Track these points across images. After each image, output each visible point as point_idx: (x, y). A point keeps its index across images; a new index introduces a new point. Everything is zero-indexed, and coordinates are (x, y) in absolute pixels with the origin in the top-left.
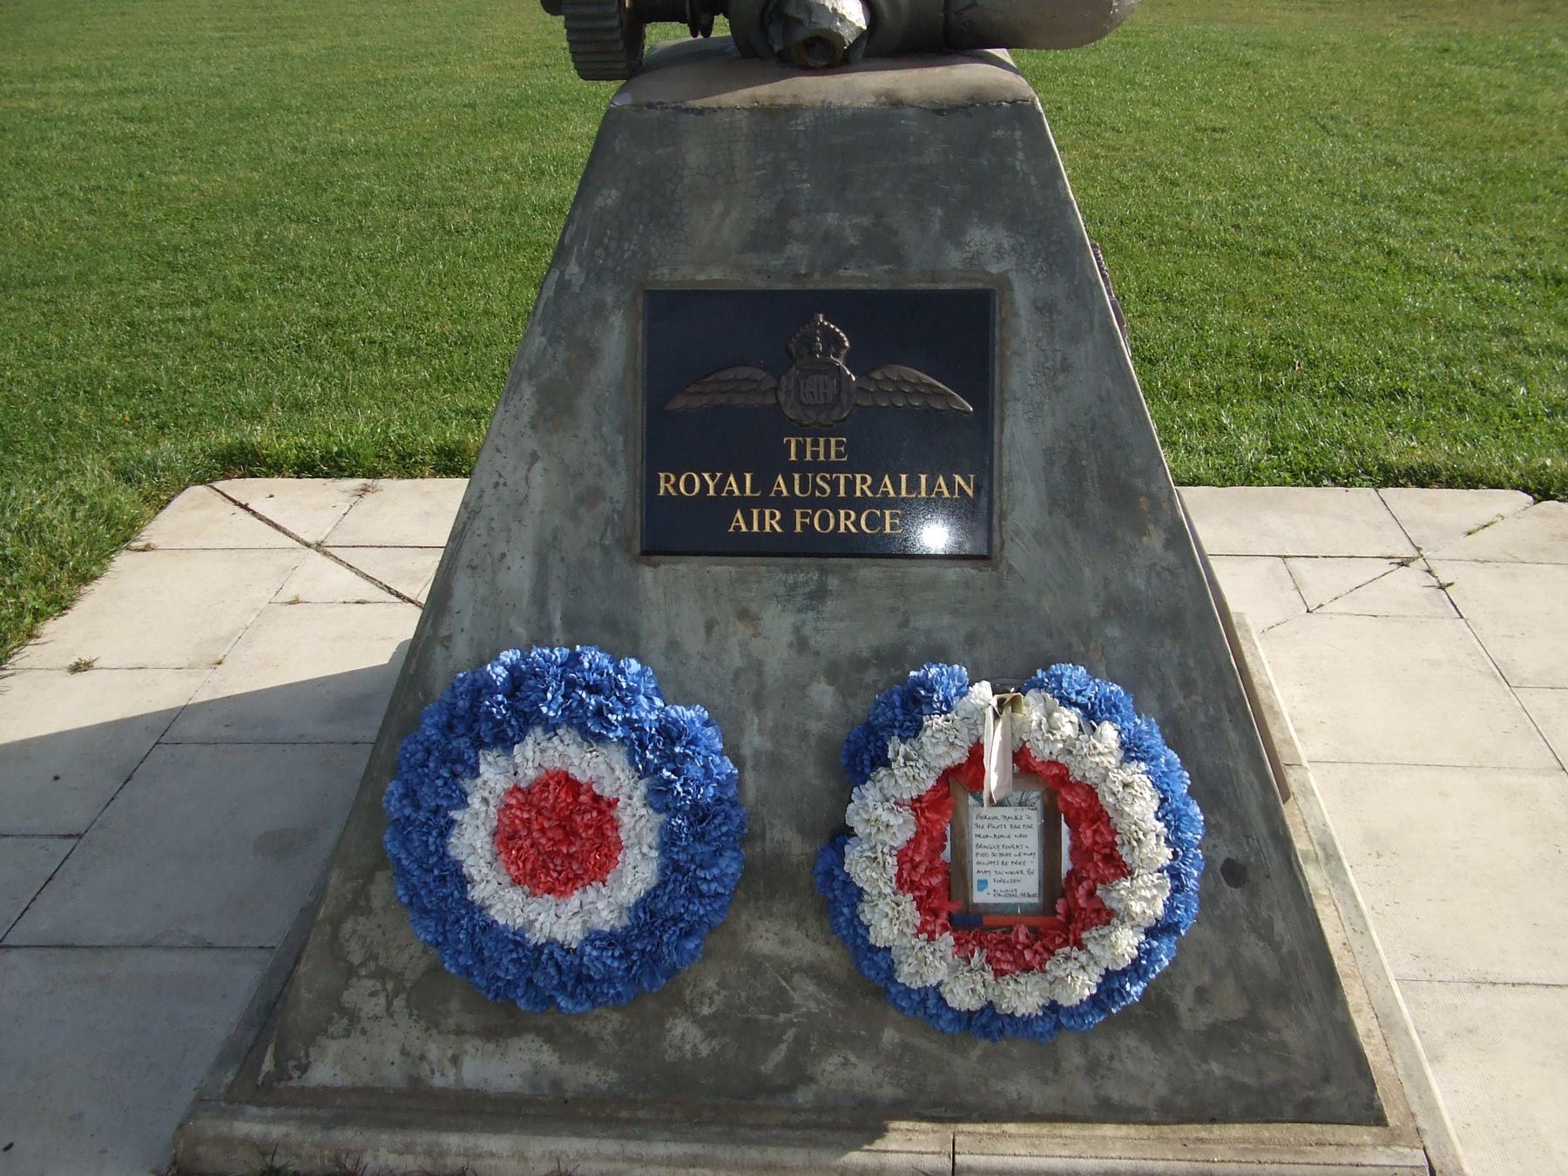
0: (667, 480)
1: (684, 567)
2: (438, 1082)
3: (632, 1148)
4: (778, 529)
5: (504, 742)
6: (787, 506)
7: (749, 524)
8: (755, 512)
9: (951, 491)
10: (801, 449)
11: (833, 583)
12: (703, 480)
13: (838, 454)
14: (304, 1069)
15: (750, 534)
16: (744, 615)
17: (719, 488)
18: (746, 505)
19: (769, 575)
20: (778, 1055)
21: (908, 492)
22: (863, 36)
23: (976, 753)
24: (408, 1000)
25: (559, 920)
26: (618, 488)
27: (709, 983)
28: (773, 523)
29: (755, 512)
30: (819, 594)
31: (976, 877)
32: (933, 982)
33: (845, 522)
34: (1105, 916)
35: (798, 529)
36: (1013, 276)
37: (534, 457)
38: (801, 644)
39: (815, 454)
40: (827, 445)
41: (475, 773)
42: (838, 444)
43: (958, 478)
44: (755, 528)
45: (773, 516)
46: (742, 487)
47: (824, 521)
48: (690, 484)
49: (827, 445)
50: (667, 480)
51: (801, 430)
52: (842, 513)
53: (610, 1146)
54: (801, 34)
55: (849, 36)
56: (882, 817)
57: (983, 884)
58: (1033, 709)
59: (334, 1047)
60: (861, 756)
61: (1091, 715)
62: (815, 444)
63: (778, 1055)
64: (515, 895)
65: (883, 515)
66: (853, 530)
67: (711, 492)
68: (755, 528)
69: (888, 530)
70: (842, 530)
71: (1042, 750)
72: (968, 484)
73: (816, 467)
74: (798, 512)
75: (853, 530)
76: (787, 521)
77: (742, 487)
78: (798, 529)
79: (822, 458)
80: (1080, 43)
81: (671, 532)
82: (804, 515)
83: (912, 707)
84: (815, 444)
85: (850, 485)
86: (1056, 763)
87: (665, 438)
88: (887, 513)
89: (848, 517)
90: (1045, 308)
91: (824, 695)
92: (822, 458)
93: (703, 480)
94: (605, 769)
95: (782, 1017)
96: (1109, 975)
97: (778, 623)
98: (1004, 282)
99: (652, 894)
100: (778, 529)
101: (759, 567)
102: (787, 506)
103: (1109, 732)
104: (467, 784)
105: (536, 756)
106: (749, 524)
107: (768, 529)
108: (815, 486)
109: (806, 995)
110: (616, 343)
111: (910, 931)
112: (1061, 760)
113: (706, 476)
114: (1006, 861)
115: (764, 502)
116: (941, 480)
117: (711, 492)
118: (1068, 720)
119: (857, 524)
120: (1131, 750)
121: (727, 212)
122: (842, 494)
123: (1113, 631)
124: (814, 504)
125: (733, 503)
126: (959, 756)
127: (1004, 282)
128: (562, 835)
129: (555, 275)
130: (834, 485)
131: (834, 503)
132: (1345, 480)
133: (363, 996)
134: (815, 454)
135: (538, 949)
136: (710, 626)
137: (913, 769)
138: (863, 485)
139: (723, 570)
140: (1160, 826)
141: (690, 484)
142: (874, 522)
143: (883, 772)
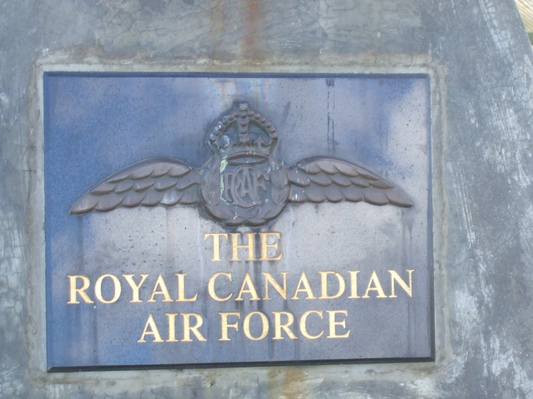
0: (80, 284)
7: (164, 334)
8: (172, 318)
9: (387, 291)
12: (123, 282)
15: (166, 345)
24: (270, 373)
28: (193, 330)
35: (225, 337)
44: (172, 338)
45: (193, 322)
47: (256, 329)
65: (326, 316)
67: (136, 298)
68: (172, 338)
69: (332, 334)
75: (87, 300)
78: (225, 337)
80: (307, 318)
82: (231, 321)
88: (332, 314)
93: (123, 282)
106: (164, 334)
107: (187, 338)
113: (129, 278)
117: (136, 298)
132: (57, 368)
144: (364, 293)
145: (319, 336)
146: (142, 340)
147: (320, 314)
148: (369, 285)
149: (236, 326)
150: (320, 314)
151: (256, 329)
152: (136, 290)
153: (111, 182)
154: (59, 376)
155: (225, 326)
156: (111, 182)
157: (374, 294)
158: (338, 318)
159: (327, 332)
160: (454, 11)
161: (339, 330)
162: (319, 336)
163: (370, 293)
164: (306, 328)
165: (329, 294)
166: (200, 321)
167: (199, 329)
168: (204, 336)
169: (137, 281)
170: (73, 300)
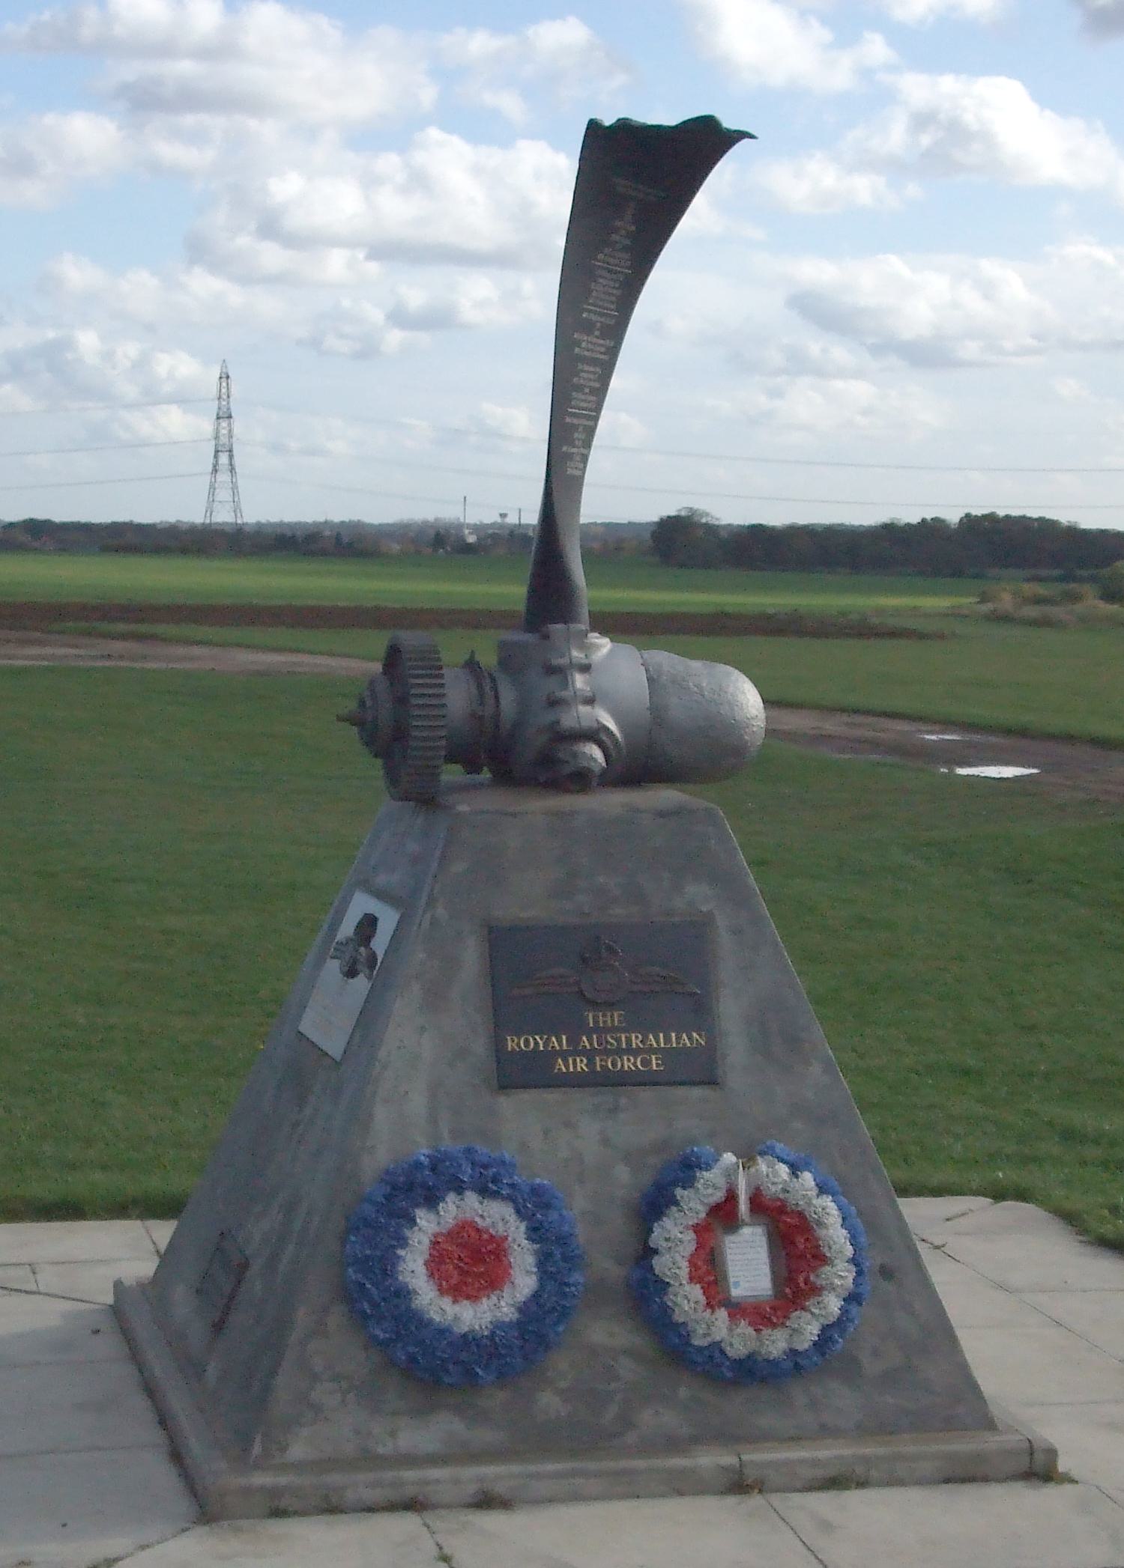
1: (527, 1096)
2: (381, 1450)
3: (532, 1468)
5: (432, 1201)
6: (590, 1055)
7: (567, 1066)
11: (623, 1101)
14: (283, 1449)
15: (568, 1072)
16: (568, 1124)
18: (564, 1055)
19: (582, 1099)
20: (612, 1412)
22: (604, 772)
23: (731, 1197)
25: (472, 1316)
26: (480, 1047)
27: (561, 1364)
28: (582, 1065)
30: (615, 1110)
31: (732, 1280)
32: (718, 1338)
33: (627, 1063)
34: (815, 1290)
36: (716, 912)
37: (423, 1029)
38: (605, 1141)
41: (412, 1222)
42: (620, 1016)
46: (560, 1044)
48: (527, 1042)
51: (594, 1005)
53: (515, 1468)
54: (567, 770)
55: (597, 770)
56: (675, 1238)
57: (737, 1284)
58: (762, 1165)
59: (305, 1432)
60: (655, 1204)
61: (795, 1169)
63: (612, 1412)
64: (446, 1302)
71: (772, 1190)
73: (606, 1030)
76: (591, 1063)
77: (560, 1044)
81: (516, 1074)
83: (687, 1169)
85: (629, 1040)
86: (779, 1199)
90: (737, 932)
91: (623, 1173)
94: (498, 1217)
95: (613, 1385)
96: (825, 1329)
97: (590, 1129)
98: (709, 918)
99: (536, 1296)
101: (576, 1094)
102: (590, 1055)
103: (807, 1178)
104: (407, 1233)
105: (453, 1209)
108: (607, 1042)
109: (627, 1369)
110: (471, 956)
111: (701, 1308)
112: (781, 1196)
114: (749, 1263)
115: (576, 1053)
116: (684, 1036)
118: (783, 1170)
119: (635, 1064)
120: (822, 1189)
122: (624, 1046)
123: (798, 1125)
124: (606, 1052)
125: (555, 1054)
126: (719, 1196)
127: (709, 918)
128: (471, 1262)
129: (428, 916)
130: (618, 1040)
131: (619, 1052)
133: (324, 1394)
134: (605, 1022)
135: (464, 1336)
136: (546, 1132)
137: (693, 1204)
138: (636, 1041)
139: (552, 1096)
140: (844, 1232)
141: (527, 1042)
142: (646, 1063)
143: (674, 1209)
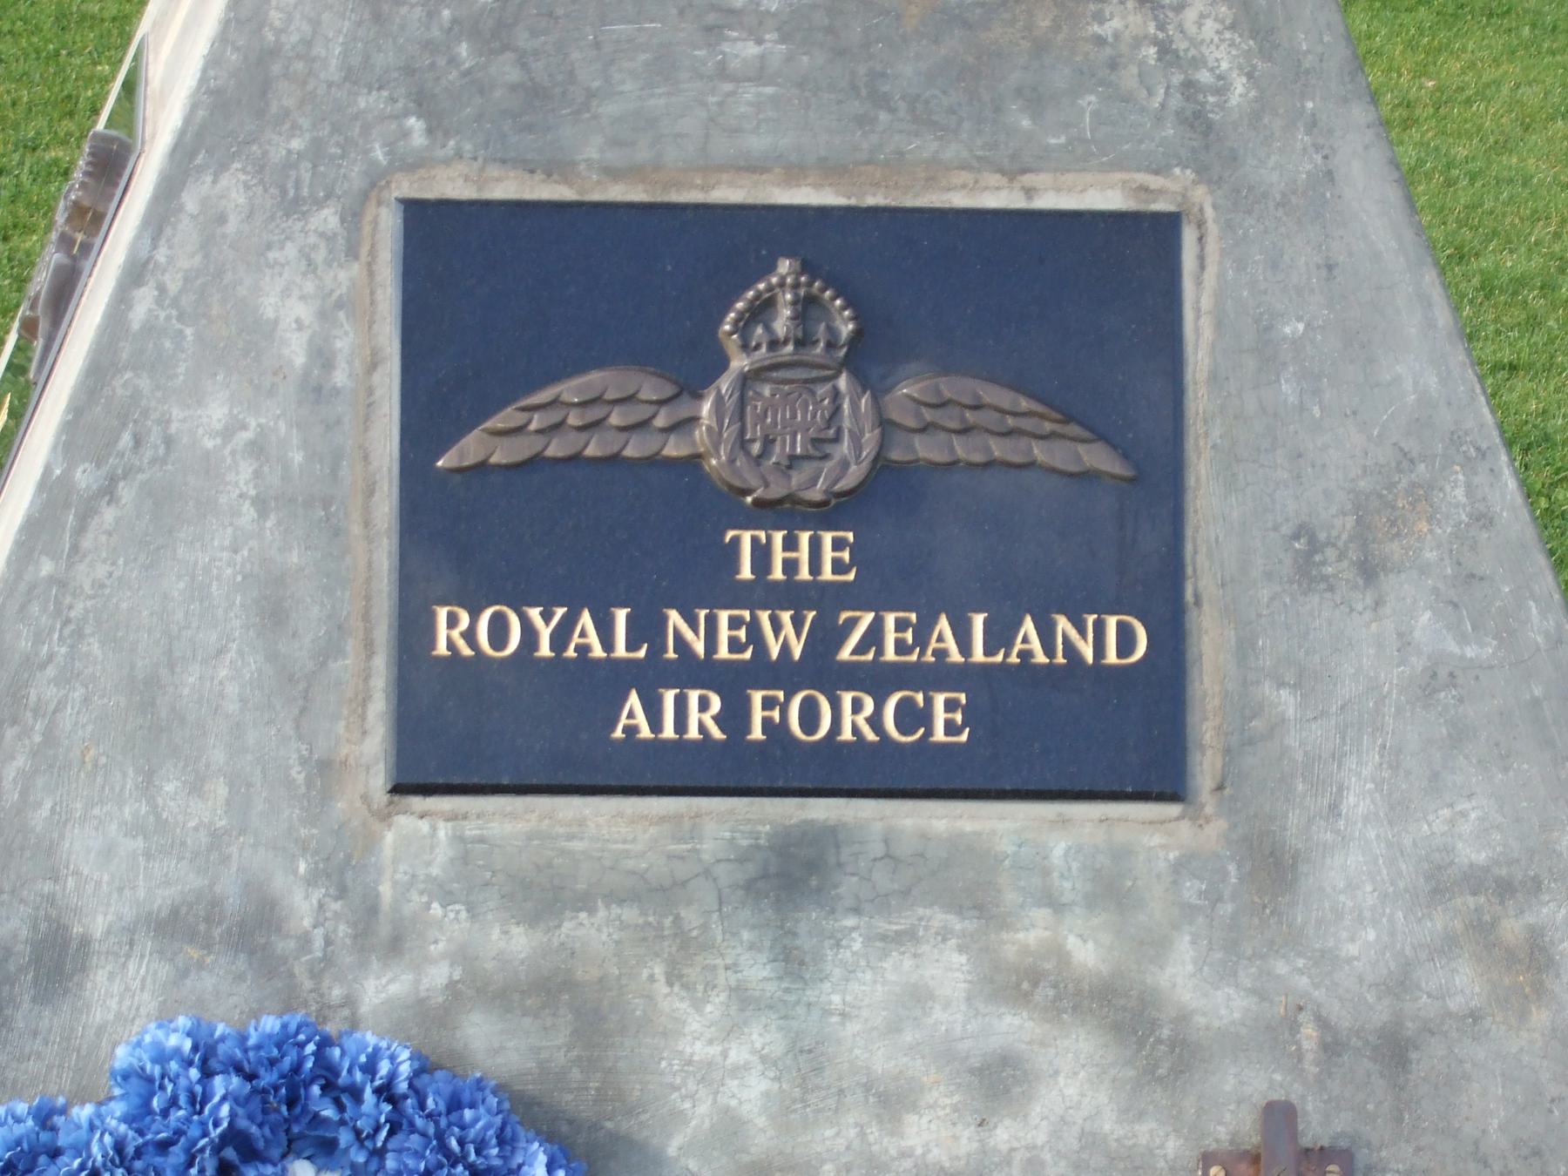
4: (717, 733)
7: (655, 723)
8: (669, 696)
9: (1049, 650)
10: (762, 555)
13: (838, 567)
15: (658, 745)
17: (560, 638)
21: (988, 652)
28: (702, 716)
29: (669, 696)
35: (757, 733)
39: (791, 566)
40: (815, 545)
42: (838, 545)
43: (1063, 624)
44: (669, 732)
45: (704, 705)
47: (810, 717)
49: (815, 545)
50: (452, 621)
52: (847, 698)
62: (791, 544)
65: (929, 701)
66: (870, 736)
67: (545, 650)
68: (669, 732)
69: (939, 735)
70: (847, 735)
72: (678, 636)
74: (757, 697)
75: (870, 736)
76: (733, 716)
78: (757, 733)
79: (804, 574)
82: (768, 704)
84: (791, 544)
87: (456, 531)
88: (940, 699)
89: (857, 707)
92: (804, 574)
100: (717, 733)
102: (732, 683)
106: (655, 723)
107: (693, 733)
113: (535, 613)
117: (545, 650)
121: (125, 775)
134: (791, 566)
142: (912, 717)
144: (565, 648)
145: (910, 739)
146: (618, 733)
147: (920, 697)
148: (1020, 638)
149: (776, 715)
150: (920, 697)
151: (810, 717)
152: (545, 634)
153: (523, 409)
154: (417, 802)
155: (758, 715)
156: (523, 409)
157: (583, 649)
158: (950, 706)
159: (929, 732)
160: (587, 115)
161: (951, 728)
162: (910, 739)
163: (935, 653)
164: (800, 718)
165: (1120, 654)
166: (716, 703)
167: (715, 718)
168: (723, 730)
169: (547, 617)
170: (442, 649)
